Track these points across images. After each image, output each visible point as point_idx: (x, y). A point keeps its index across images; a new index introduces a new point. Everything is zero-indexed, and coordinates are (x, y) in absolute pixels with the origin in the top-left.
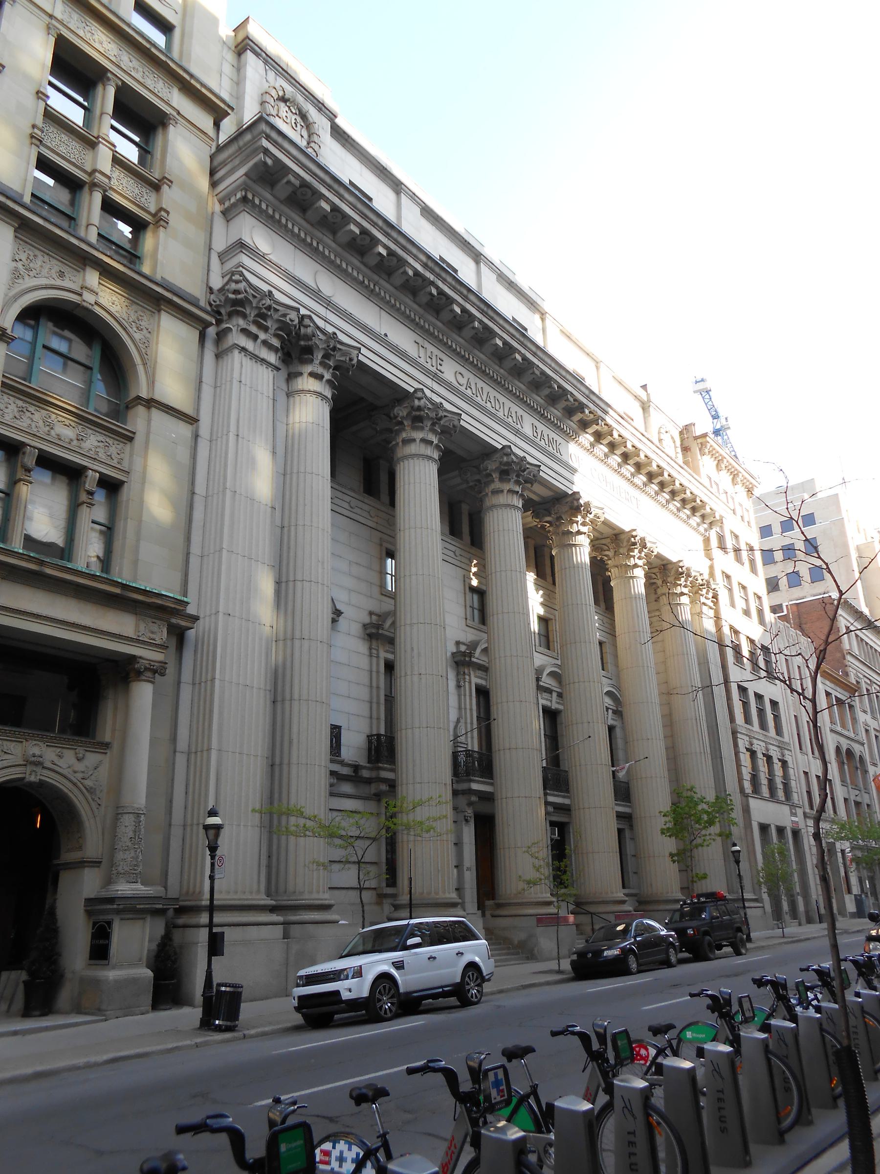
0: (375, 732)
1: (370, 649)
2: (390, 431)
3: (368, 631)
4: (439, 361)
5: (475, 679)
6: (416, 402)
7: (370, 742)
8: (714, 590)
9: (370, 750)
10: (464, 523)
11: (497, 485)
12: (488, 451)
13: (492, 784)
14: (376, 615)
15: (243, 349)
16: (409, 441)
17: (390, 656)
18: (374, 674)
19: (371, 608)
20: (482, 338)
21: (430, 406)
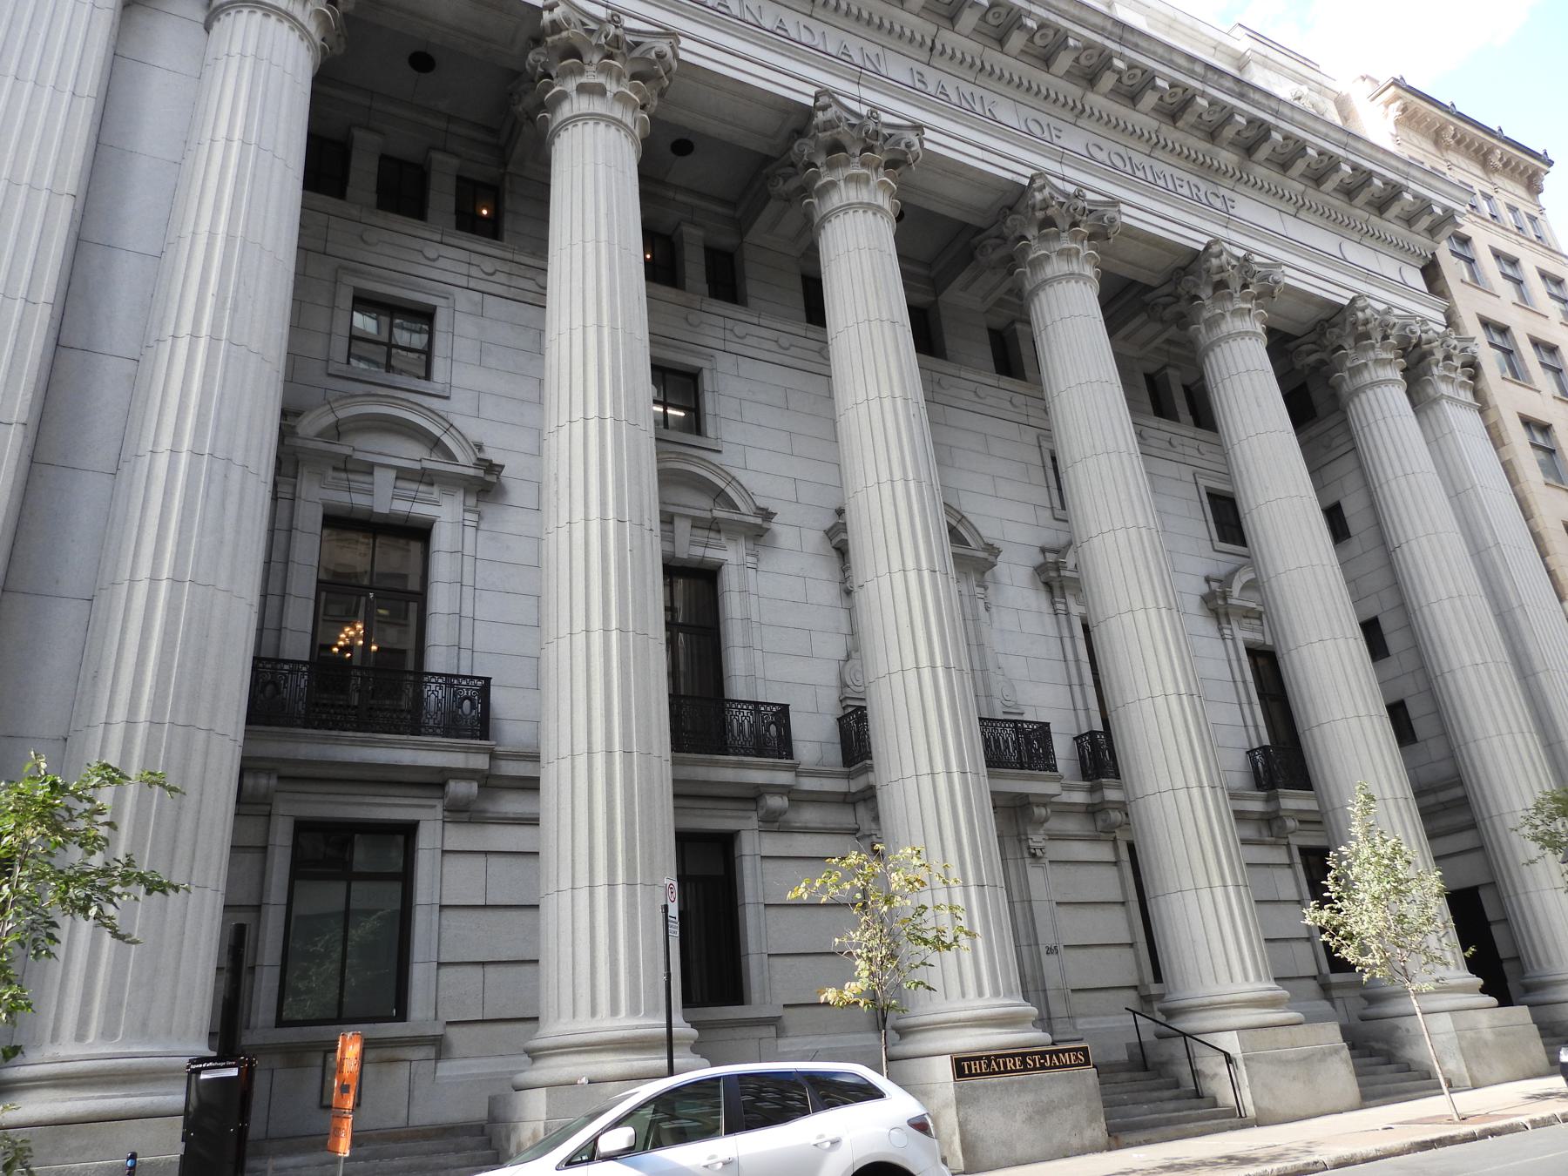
0: (1085, 730)
1: (1220, 630)
4: (1054, 132)
5: (1244, 634)
6: (1039, 196)
7: (1080, 746)
8: (1265, 278)
9: (1082, 758)
10: (1170, 393)
11: (1037, 251)
12: (798, 121)
18: (1067, 642)
19: (1205, 573)
20: (1289, 157)
21: (1234, 262)
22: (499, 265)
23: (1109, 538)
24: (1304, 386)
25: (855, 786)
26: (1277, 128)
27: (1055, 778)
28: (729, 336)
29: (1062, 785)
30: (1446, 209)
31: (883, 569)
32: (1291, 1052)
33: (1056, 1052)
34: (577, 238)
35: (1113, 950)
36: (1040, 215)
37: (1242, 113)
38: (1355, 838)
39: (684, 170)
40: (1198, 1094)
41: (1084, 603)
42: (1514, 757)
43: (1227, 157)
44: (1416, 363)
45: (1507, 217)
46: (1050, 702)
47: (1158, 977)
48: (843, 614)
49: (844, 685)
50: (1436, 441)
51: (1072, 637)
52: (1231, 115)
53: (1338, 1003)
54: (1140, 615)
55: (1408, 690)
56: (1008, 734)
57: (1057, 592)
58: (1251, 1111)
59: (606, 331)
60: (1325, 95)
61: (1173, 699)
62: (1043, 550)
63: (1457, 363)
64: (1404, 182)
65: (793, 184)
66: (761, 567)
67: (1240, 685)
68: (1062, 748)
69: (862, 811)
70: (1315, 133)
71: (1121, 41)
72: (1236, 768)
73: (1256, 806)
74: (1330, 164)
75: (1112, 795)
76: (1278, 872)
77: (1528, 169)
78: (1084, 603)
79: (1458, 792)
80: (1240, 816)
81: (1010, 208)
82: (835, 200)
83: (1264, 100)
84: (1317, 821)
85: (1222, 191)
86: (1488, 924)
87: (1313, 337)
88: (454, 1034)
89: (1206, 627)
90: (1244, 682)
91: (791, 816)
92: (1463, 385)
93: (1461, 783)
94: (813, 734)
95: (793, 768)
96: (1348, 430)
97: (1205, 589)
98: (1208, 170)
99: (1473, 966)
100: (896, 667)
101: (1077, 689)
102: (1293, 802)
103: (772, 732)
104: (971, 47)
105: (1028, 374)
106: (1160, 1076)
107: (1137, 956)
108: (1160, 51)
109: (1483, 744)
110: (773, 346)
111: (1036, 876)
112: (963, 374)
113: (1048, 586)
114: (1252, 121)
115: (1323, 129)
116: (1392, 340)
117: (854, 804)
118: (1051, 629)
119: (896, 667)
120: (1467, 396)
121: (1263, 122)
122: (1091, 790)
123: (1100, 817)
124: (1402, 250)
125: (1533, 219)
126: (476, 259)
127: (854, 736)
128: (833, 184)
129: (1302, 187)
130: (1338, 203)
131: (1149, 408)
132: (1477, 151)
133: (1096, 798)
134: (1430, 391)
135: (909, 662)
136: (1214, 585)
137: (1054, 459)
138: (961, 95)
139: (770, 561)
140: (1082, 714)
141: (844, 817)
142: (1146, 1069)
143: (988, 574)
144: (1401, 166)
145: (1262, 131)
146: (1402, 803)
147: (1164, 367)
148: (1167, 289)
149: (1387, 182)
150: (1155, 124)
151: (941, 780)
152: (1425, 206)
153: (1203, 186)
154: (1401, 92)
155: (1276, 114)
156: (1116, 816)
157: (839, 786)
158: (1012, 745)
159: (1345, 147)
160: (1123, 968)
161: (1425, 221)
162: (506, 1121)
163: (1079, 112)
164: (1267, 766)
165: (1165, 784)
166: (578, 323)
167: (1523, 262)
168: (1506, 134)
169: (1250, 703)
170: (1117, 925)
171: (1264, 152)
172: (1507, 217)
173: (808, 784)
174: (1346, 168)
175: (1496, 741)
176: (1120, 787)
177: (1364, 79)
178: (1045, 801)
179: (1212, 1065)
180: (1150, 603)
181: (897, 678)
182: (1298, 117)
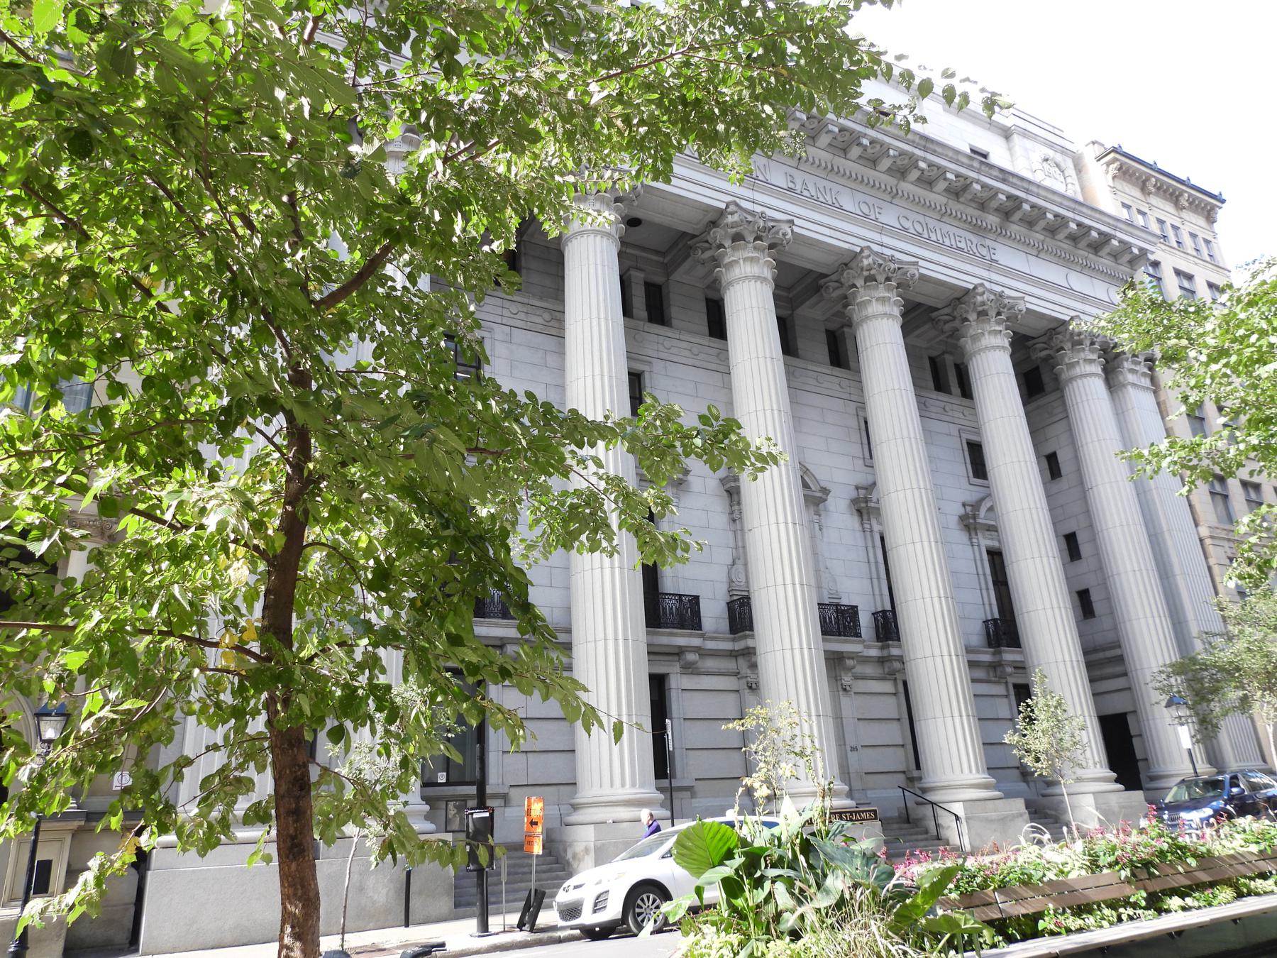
1: (970, 539)
2: (714, 259)
3: (727, 486)
5: (985, 542)
6: (979, 298)
7: (987, 628)
10: (942, 372)
13: (1021, 653)
14: (862, 488)
15: (1134, 385)
16: (731, 264)
17: (995, 544)
18: (870, 549)
22: (520, 307)
23: (901, 495)
24: (1037, 368)
25: (739, 646)
26: (1027, 201)
27: (861, 636)
28: (661, 348)
29: (864, 646)
30: (1141, 249)
31: (764, 521)
32: (994, 815)
33: (859, 812)
34: (587, 315)
35: (891, 749)
36: (866, 273)
37: (1003, 192)
38: (1036, 695)
39: (639, 234)
40: (938, 838)
41: (880, 523)
42: (1153, 632)
43: (992, 220)
44: (1111, 361)
45: (1188, 241)
46: (861, 596)
47: (918, 767)
48: (731, 534)
49: (731, 581)
50: (1121, 414)
51: (874, 547)
52: (996, 194)
53: (1032, 784)
54: (918, 546)
55: (1089, 582)
56: (831, 612)
57: (865, 517)
58: (968, 848)
59: (606, 379)
60: (1066, 154)
61: (936, 600)
62: (857, 488)
63: (1141, 359)
64: (1113, 232)
65: (708, 254)
66: (682, 505)
67: (982, 577)
68: (865, 620)
69: (741, 661)
70: (1053, 203)
71: (925, 149)
72: (976, 628)
73: (986, 658)
74: (1061, 221)
75: (895, 651)
76: (998, 700)
77: (1206, 205)
78: (880, 523)
79: (1118, 652)
80: (972, 664)
81: (846, 265)
82: (737, 272)
83: (1019, 183)
84: (1021, 667)
85: (988, 242)
86: (1131, 737)
87: (1044, 339)
88: (514, 793)
89: (962, 537)
90: (876, 562)
91: (700, 664)
92: (1144, 374)
93: (1120, 647)
94: (713, 613)
95: (702, 636)
96: (1064, 404)
97: (962, 511)
98: (979, 230)
99: (1113, 765)
100: (771, 583)
101: (875, 581)
102: (1009, 655)
103: (687, 613)
104: (825, 156)
105: (852, 364)
106: (917, 826)
107: (906, 752)
108: (950, 154)
109: (1134, 622)
110: (686, 353)
111: (845, 701)
112: (810, 367)
113: (859, 512)
114: (1010, 197)
115: (1059, 200)
116: (1097, 346)
117: (736, 657)
118: (860, 542)
119: (771, 583)
120: (1146, 382)
121: (1017, 198)
122: (882, 648)
123: (887, 665)
124: (1112, 278)
125: (1207, 242)
126: (507, 304)
127: (740, 615)
128: (736, 262)
129: (1042, 237)
130: (1067, 246)
131: (931, 384)
132: (1171, 194)
133: (885, 653)
134: (1121, 378)
135: (780, 581)
136: (968, 509)
137: (866, 423)
138: (818, 189)
139: (690, 501)
140: (878, 598)
141: (730, 665)
142: (908, 822)
143: (821, 506)
144: (1111, 222)
145: (1016, 202)
146: (1075, 664)
147: (943, 353)
148: (947, 311)
149: (1100, 233)
150: (944, 200)
151: (797, 652)
152: (1126, 247)
153: (975, 239)
154: (1118, 156)
155: (1027, 191)
156: (897, 665)
157: (728, 646)
158: (837, 620)
159: (1073, 211)
160: (898, 760)
161: (1127, 257)
162: (563, 842)
163: (894, 195)
164: (996, 632)
165: (928, 653)
166: (589, 373)
167: (1197, 278)
168: (1193, 182)
169: (987, 589)
170: (895, 733)
171: (1017, 216)
172: (1188, 241)
173: (710, 645)
174: (1094, 234)
175: (1143, 621)
176: (900, 646)
177: (1094, 143)
178: (852, 656)
179: (947, 821)
180: (925, 538)
181: (772, 590)
182: (1042, 192)
